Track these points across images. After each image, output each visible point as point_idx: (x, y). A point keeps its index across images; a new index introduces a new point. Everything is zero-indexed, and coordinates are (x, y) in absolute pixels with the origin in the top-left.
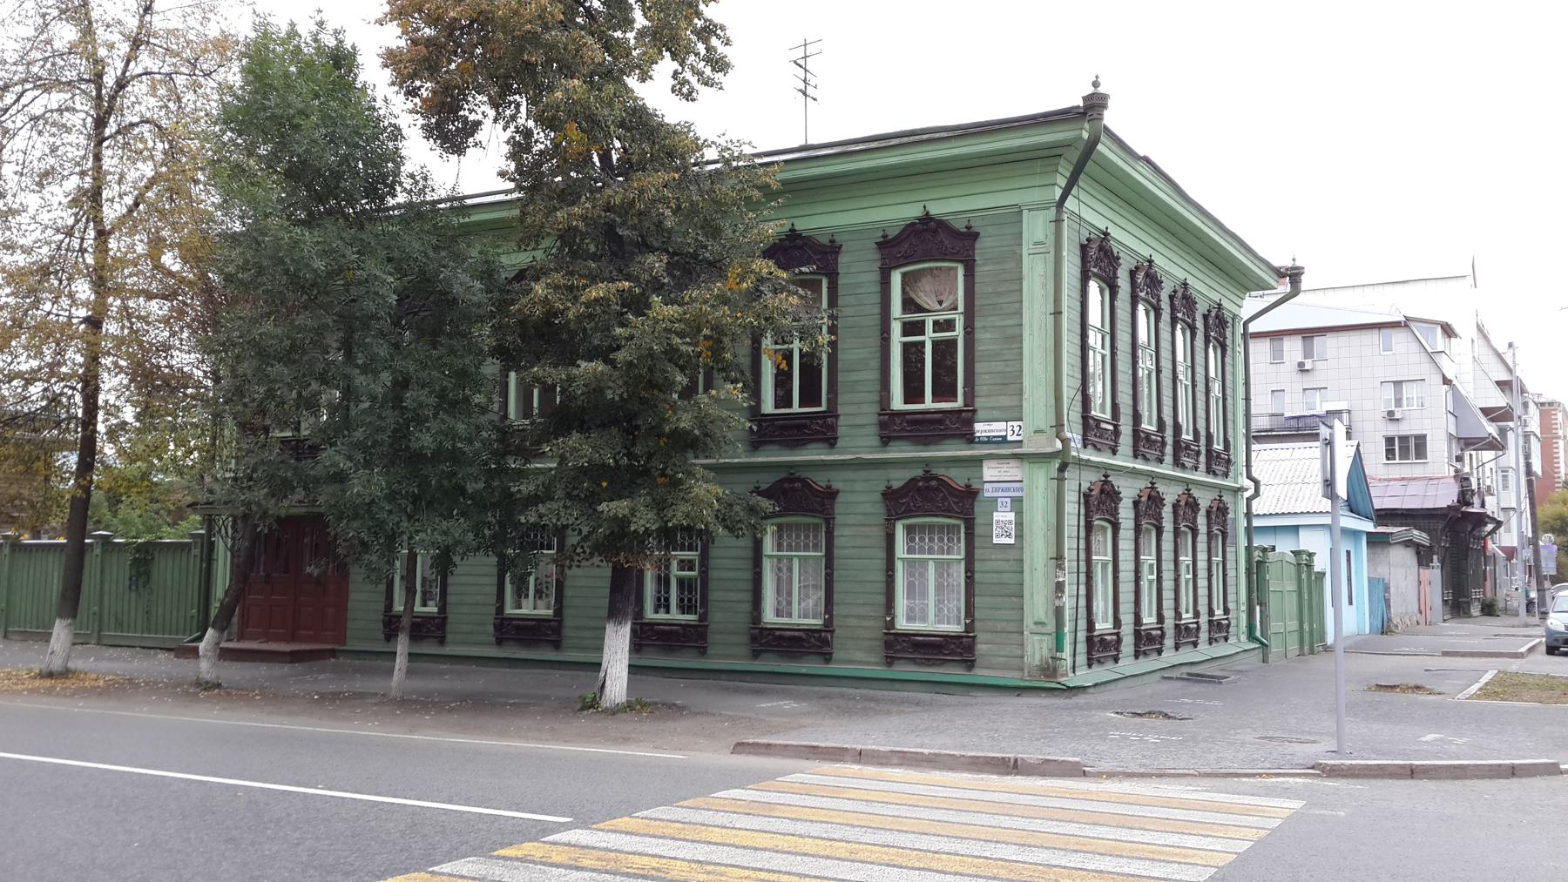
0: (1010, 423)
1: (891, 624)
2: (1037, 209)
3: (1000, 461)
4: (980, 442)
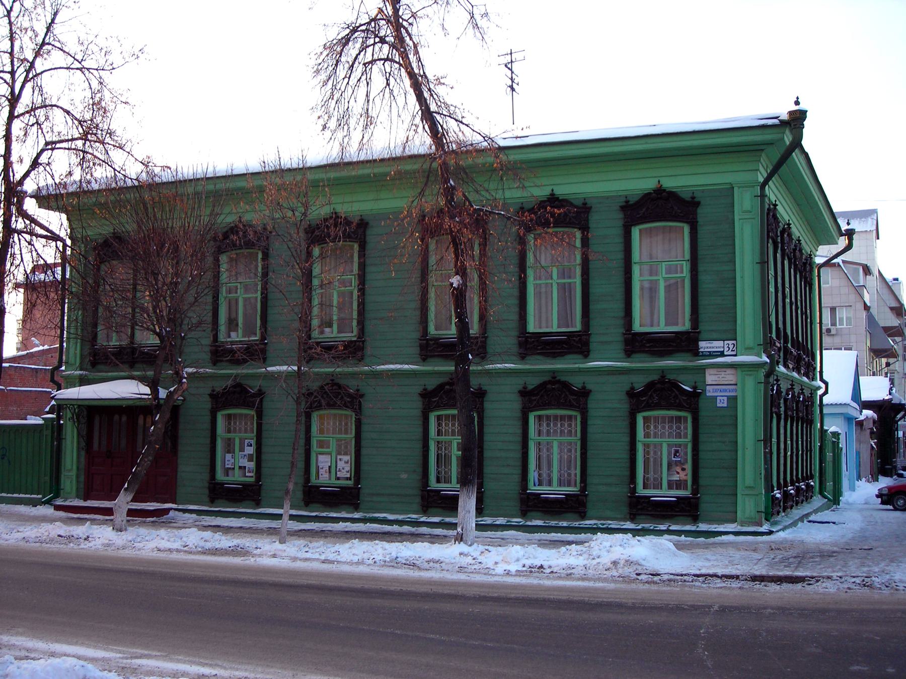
0: (726, 342)
1: (634, 490)
2: (746, 187)
3: (719, 370)
4: (702, 356)
